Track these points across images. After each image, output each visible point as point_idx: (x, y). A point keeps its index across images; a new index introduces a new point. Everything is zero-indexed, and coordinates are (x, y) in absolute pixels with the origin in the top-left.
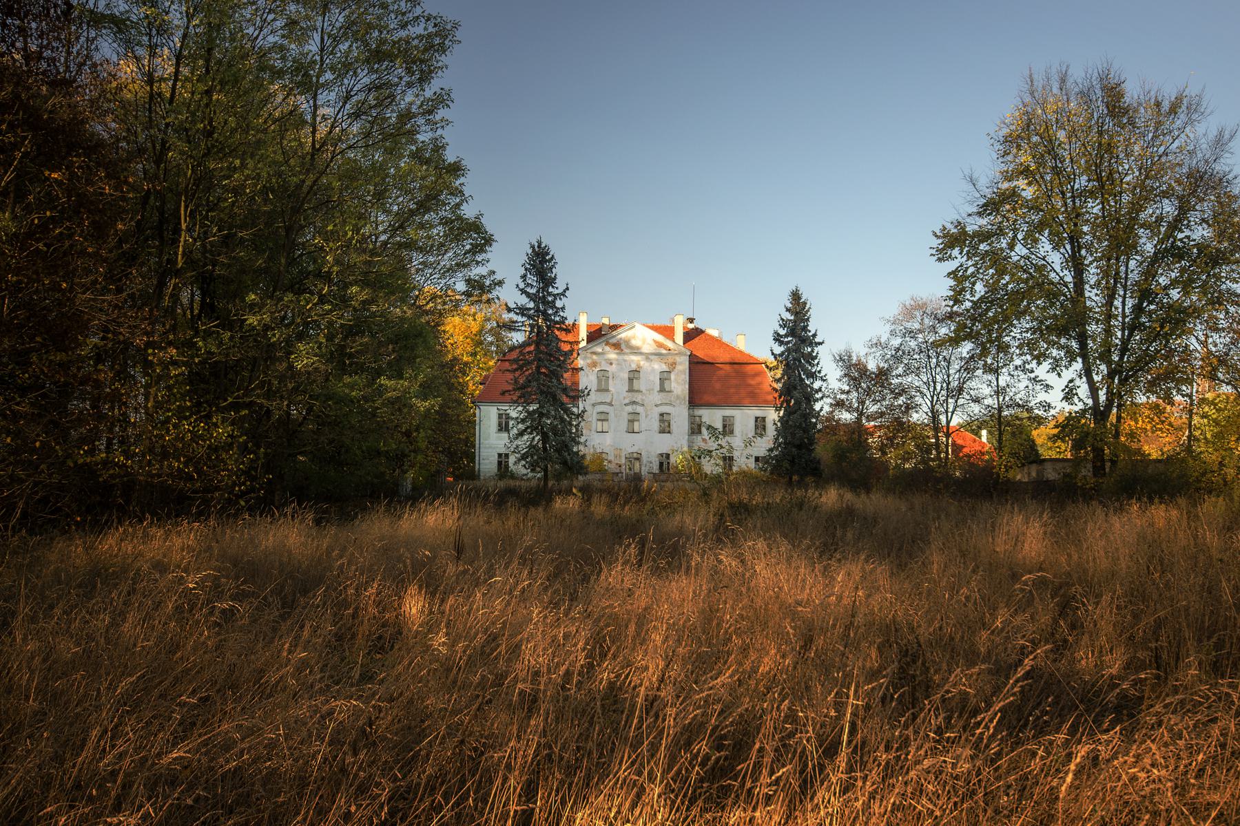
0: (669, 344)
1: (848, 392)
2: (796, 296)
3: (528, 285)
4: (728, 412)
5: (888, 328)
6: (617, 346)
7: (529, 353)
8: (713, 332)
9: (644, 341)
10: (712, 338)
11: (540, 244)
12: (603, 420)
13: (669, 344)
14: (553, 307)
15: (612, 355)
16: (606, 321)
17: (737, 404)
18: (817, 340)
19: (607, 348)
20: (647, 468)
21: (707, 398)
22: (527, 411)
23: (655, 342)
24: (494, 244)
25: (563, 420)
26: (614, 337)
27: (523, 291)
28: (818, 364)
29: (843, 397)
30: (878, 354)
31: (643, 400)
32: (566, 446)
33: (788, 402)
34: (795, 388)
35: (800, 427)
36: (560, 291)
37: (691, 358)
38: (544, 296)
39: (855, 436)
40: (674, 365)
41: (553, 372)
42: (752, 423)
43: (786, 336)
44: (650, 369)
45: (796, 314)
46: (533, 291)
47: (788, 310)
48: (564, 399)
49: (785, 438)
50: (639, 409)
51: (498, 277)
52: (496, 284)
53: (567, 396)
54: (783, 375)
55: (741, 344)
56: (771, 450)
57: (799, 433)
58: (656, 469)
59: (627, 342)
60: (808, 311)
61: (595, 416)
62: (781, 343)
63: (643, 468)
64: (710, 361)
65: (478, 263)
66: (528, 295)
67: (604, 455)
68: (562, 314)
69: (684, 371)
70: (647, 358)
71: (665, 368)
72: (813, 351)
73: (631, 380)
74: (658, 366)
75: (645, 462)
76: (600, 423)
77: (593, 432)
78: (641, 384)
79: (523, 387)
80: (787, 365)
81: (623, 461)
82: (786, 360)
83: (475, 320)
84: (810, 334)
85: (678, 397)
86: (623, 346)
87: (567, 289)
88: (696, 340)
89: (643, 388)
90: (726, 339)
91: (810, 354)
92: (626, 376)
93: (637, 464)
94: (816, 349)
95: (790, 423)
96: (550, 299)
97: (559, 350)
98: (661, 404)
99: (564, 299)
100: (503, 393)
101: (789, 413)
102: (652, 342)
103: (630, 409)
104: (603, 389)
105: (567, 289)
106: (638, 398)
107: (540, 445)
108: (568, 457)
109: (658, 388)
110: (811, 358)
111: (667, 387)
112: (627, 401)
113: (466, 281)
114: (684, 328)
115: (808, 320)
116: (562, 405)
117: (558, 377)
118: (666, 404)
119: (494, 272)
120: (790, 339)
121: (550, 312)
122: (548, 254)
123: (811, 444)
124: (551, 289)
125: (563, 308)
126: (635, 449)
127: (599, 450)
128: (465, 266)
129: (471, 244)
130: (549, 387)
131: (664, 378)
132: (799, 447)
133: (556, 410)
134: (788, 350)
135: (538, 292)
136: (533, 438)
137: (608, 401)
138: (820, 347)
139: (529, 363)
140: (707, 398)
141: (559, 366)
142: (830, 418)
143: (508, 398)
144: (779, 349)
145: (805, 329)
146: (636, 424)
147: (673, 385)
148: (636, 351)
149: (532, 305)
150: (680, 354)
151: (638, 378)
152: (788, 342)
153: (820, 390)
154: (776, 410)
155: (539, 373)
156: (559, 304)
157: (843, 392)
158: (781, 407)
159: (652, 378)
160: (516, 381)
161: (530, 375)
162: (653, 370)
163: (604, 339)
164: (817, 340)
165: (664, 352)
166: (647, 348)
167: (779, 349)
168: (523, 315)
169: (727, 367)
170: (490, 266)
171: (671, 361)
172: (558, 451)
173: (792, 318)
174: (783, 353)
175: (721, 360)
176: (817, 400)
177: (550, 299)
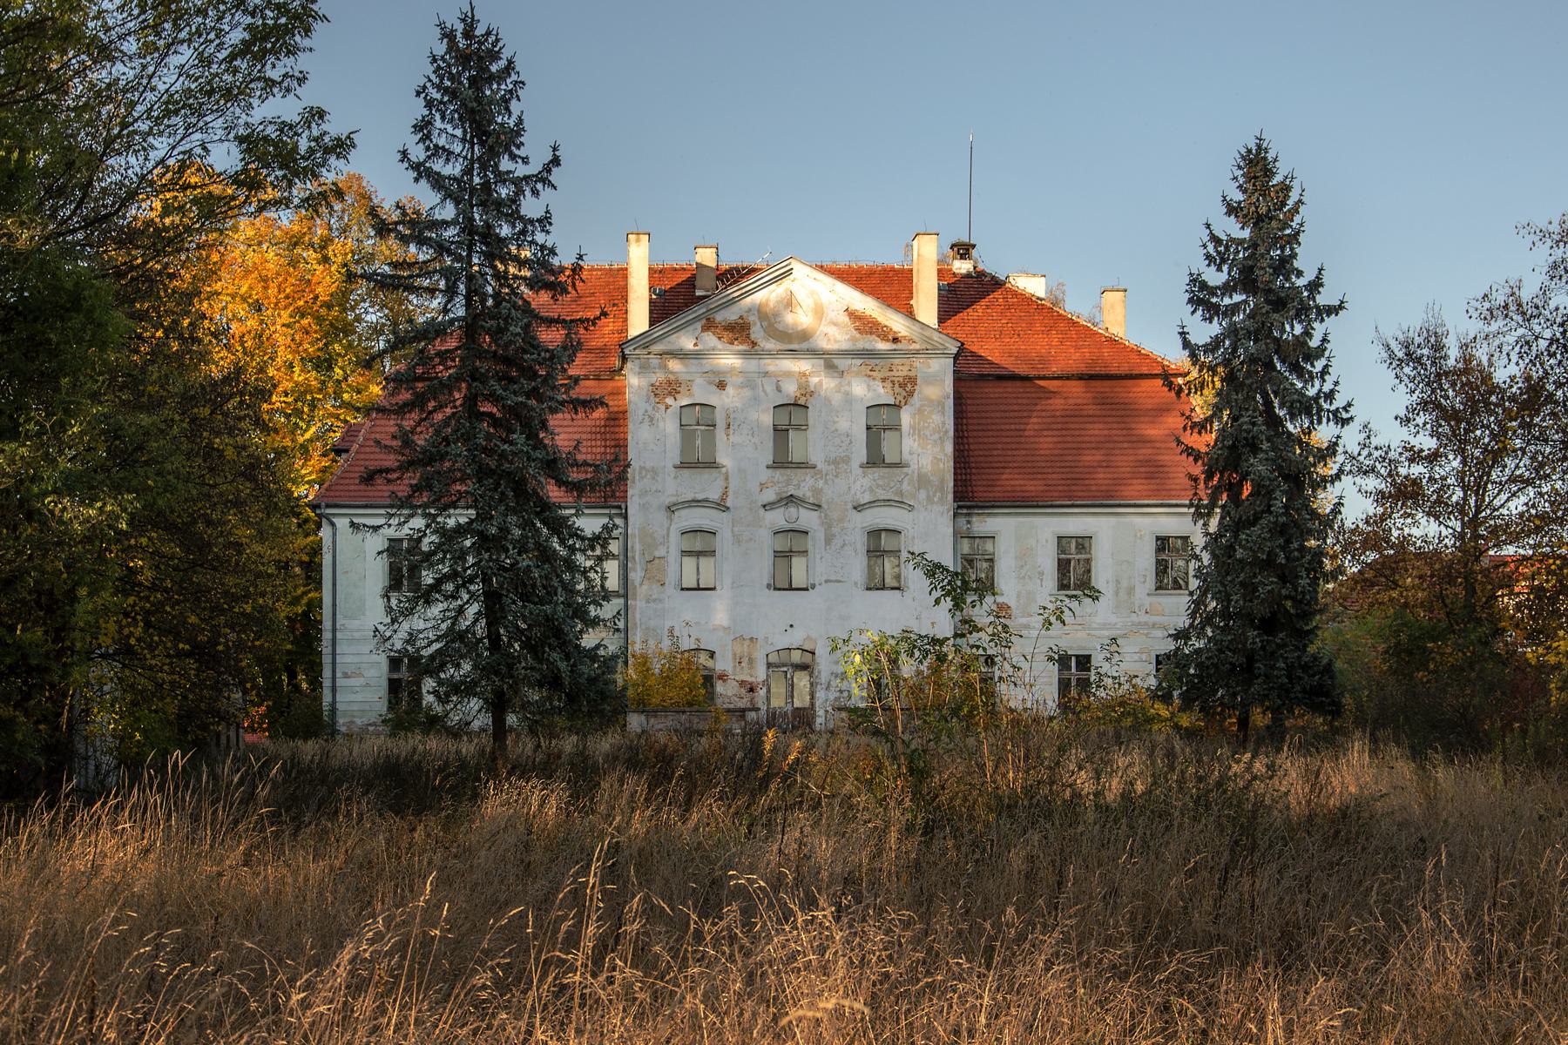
0: (895, 322)
1: (1433, 457)
2: (1257, 166)
3: (437, 151)
4: (1075, 524)
5: (1544, 255)
6: (738, 331)
7: (443, 356)
8: (1034, 286)
9: (819, 312)
10: (1027, 300)
11: (470, 23)
12: (698, 554)
13: (895, 322)
14: (514, 217)
15: (728, 359)
16: (707, 257)
17: (1105, 499)
18: (1322, 300)
19: (710, 340)
20: (832, 695)
21: (1011, 480)
22: (442, 531)
23: (853, 315)
24: (318, 27)
25: (546, 555)
26: (733, 301)
27: (421, 171)
28: (1325, 371)
29: (1417, 470)
30: (1511, 339)
31: (818, 492)
32: (558, 633)
33: (1234, 490)
34: (1255, 449)
35: (1269, 564)
36: (533, 168)
37: (962, 356)
38: (486, 186)
39: (1457, 592)
40: (908, 385)
41: (515, 412)
42: (1146, 559)
43: (1227, 289)
44: (837, 399)
45: (1258, 221)
46: (453, 169)
47: (1232, 210)
48: (554, 493)
49: (1224, 598)
50: (807, 519)
51: (334, 127)
52: (328, 151)
53: (560, 483)
54: (1217, 410)
55: (1116, 319)
56: (1181, 635)
57: (1268, 584)
58: (858, 695)
59: (769, 319)
60: (1295, 210)
61: (675, 543)
62: (1212, 311)
63: (820, 695)
64: (1022, 370)
65: (270, 84)
66: (437, 182)
67: (703, 659)
68: (540, 238)
69: (941, 404)
70: (830, 367)
71: (883, 394)
72: (1307, 333)
73: (780, 432)
74: (864, 390)
75: (824, 678)
76: (689, 563)
77: (670, 590)
78: (811, 445)
79: (429, 458)
80: (1230, 378)
81: (761, 673)
82: (1226, 363)
83: (325, 260)
84: (1301, 282)
85: (922, 481)
86: (756, 332)
87: (556, 161)
88: (976, 312)
89: (816, 457)
90: (1076, 306)
91: (1301, 342)
92: (767, 419)
93: (802, 681)
94: (1319, 330)
95: (1240, 553)
96: (504, 192)
97: (533, 344)
98: (872, 504)
99: (546, 194)
100: (369, 478)
101: (1236, 525)
102: (845, 319)
103: (778, 518)
104: (697, 461)
105: (556, 161)
106: (804, 485)
107: (481, 629)
108: (563, 665)
109: (860, 453)
110: (1303, 355)
111: (889, 453)
112: (770, 495)
113: (241, 140)
114: (941, 273)
115: (1294, 238)
116: (545, 509)
117: (533, 428)
118: (887, 502)
119: (321, 114)
120: (1238, 298)
121: (505, 230)
122: (495, 56)
123: (1306, 616)
124: (505, 164)
125: (545, 221)
126: (796, 638)
127: (686, 644)
128: (229, 94)
129: (249, 28)
130: (503, 455)
131: (880, 423)
132: (1268, 625)
133: (527, 525)
134: (1232, 331)
135: (468, 171)
136: (461, 611)
137: (714, 495)
138: (1330, 321)
139: (448, 386)
140: (1011, 480)
141: (534, 393)
142: (1374, 535)
143: (381, 488)
144: (1204, 331)
145: (1284, 266)
146: (798, 564)
147: (909, 444)
148: (798, 343)
149: (448, 212)
150: (929, 352)
151: (802, 427)
152: (1234, 309)
153: (1332, 449)
154: (1198, 515)
155: (474, 415)
156: (531, 207)
157: (1415, 456)
158: (1213, 505)
159: (843, 424)
160: (406, 439)
161: (446, 422)
162: (849, 399)
163: (700, 310)
164: (1322, 300)
165: (882, 346)
166: (835, 335)
167: (1204, 331)
168: (422, 241)
169: (1076, 388)
170: (310, 95)
171: (901, 372)
172: (531, 647)
173: (1246, 234)
174: (1216, 343)
175: (1055, 369)
176: (1325, 482)
177: (504, 192)
